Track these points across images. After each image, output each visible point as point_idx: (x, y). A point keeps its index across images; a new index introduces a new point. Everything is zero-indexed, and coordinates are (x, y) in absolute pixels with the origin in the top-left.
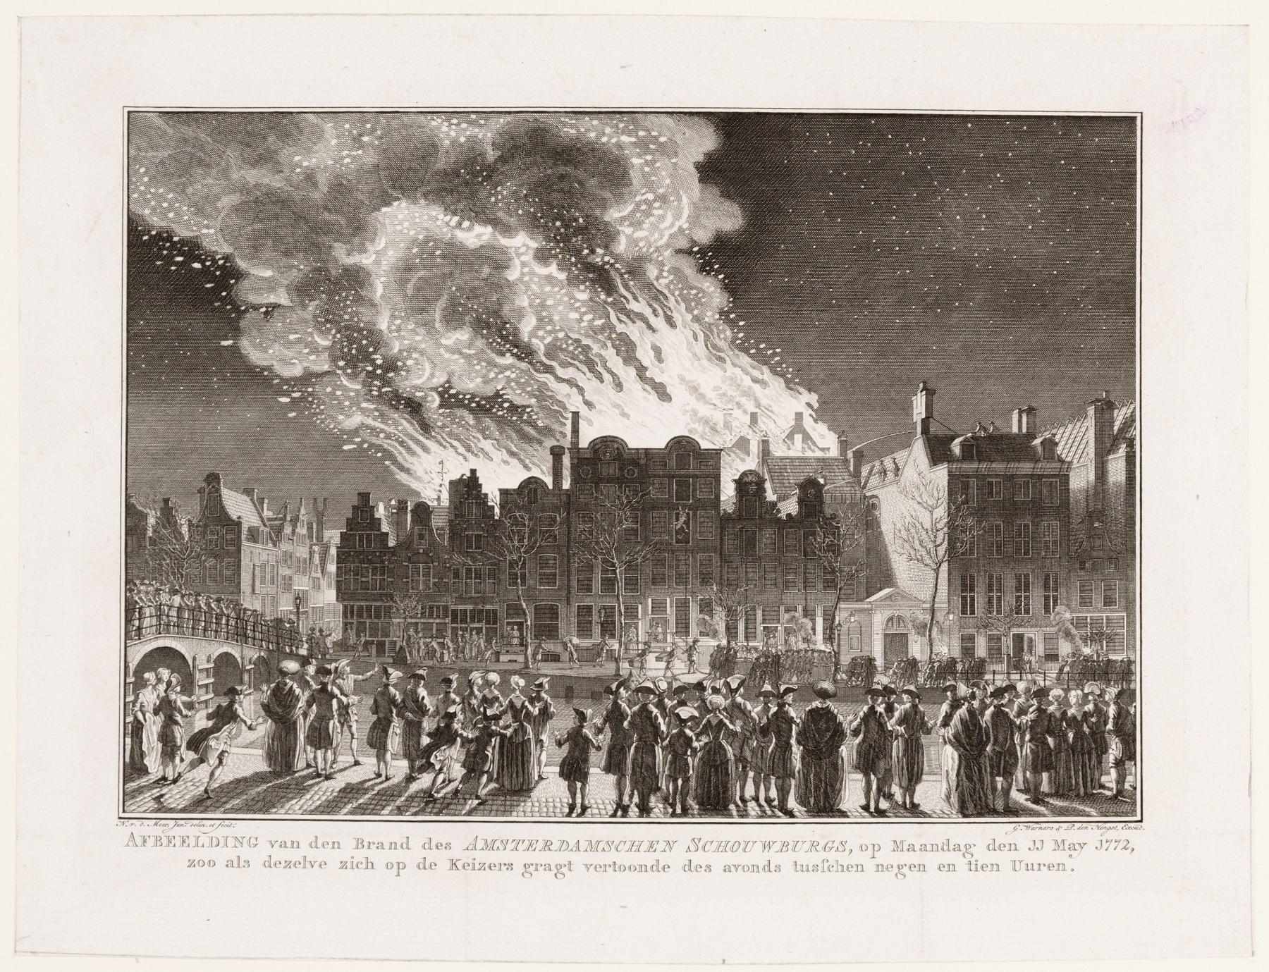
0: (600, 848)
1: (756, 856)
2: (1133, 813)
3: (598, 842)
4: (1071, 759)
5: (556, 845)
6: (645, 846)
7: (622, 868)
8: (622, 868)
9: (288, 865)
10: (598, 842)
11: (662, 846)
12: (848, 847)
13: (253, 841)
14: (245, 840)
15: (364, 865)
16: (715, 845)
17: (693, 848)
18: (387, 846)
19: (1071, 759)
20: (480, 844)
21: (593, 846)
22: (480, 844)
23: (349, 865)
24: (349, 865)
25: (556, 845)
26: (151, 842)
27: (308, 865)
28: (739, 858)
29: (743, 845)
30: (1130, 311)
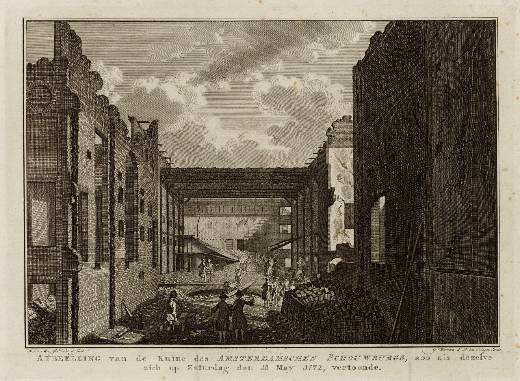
0: (283, 359)
1: (362, 362)
2: (29, 343)
3: (282, 357)
4: (45, 329)
5: (261, 358)
6: (302, 358)
7: (354, 368)
8: (354, 368)
9: (473, 358)
10: (282, 357)
11: (310, 358)
12: (405, 358)
13: (98, 358)
14: (94, 358)
15: (156, 369)
16: (295, 358)
17: (330, 359)
18: (121, 359)
19: (45, 329)
20: (225, 358)
21: (279, 358)
22: (225, 358)
23: (148, 368)
24: (148, 368)
25: (261, 358)
26: (51, 359)
27: (483, 358)
28: (353, 363)
29: (354, 357)
30: (496, 327)
